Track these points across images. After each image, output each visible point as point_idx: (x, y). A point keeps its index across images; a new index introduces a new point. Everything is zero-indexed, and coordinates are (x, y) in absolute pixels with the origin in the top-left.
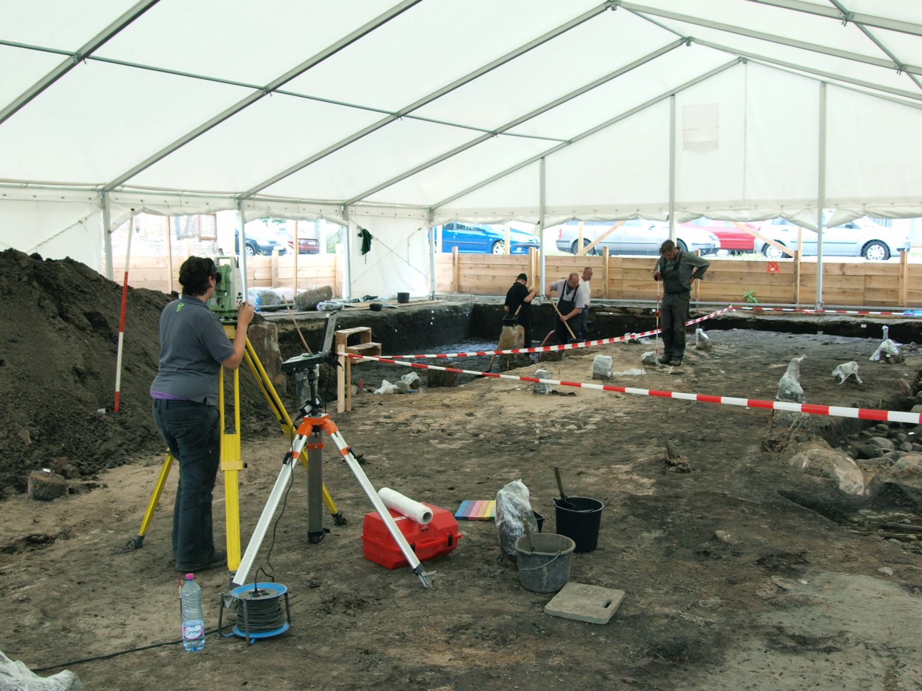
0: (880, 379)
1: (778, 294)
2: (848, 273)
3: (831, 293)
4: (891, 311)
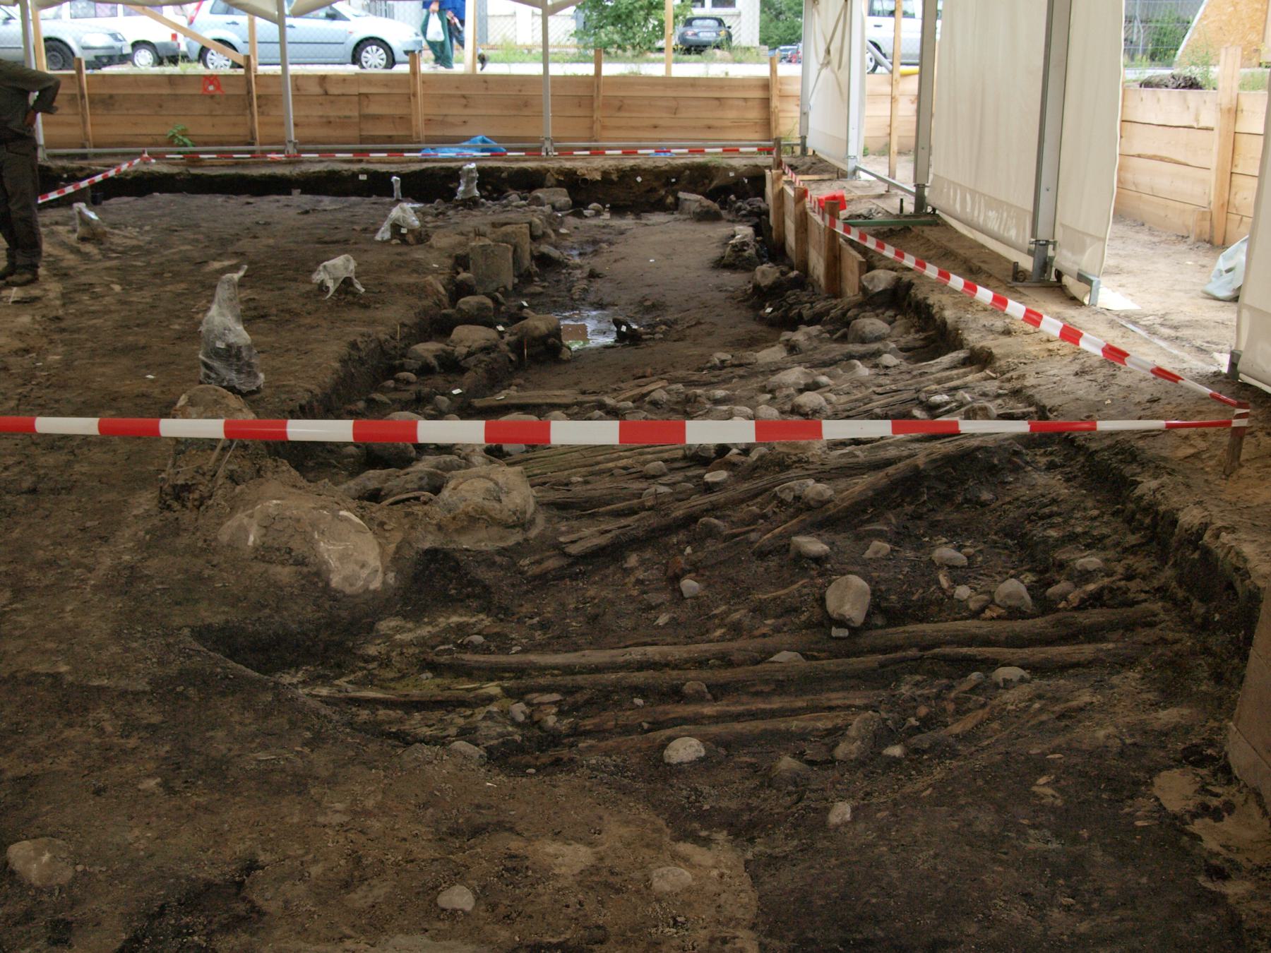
0: (395, 279)
1: (224, 131)
2: (334, 90)
3: (309, 125)
4: (403, 151)
